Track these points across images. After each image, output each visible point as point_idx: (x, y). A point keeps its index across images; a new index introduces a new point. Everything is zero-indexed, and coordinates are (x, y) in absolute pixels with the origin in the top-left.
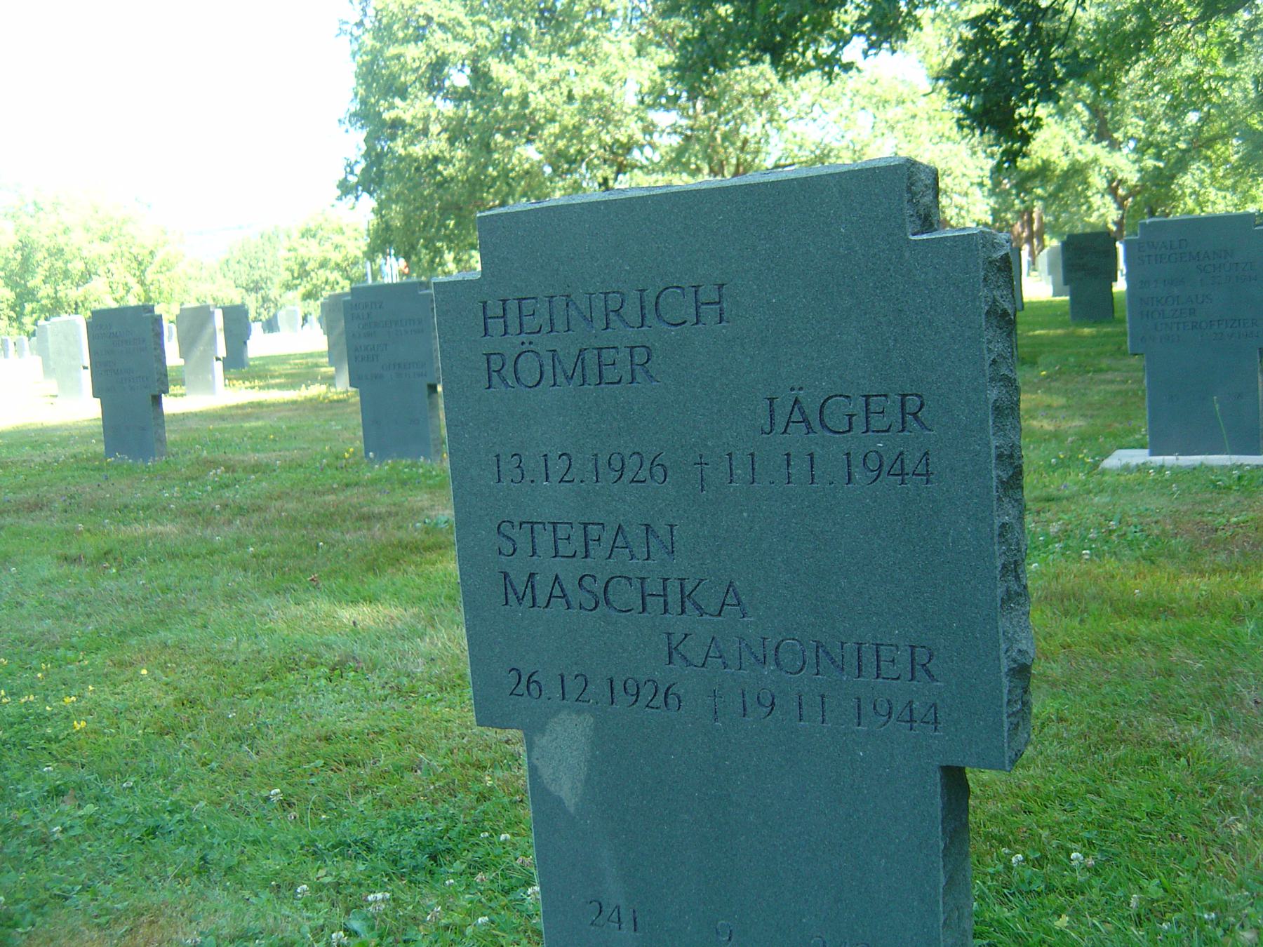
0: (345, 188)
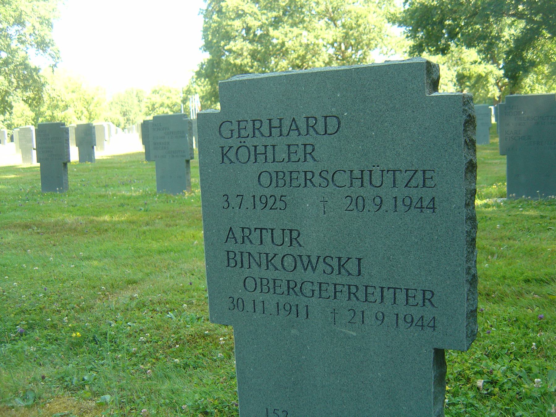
0: (199, 75)
